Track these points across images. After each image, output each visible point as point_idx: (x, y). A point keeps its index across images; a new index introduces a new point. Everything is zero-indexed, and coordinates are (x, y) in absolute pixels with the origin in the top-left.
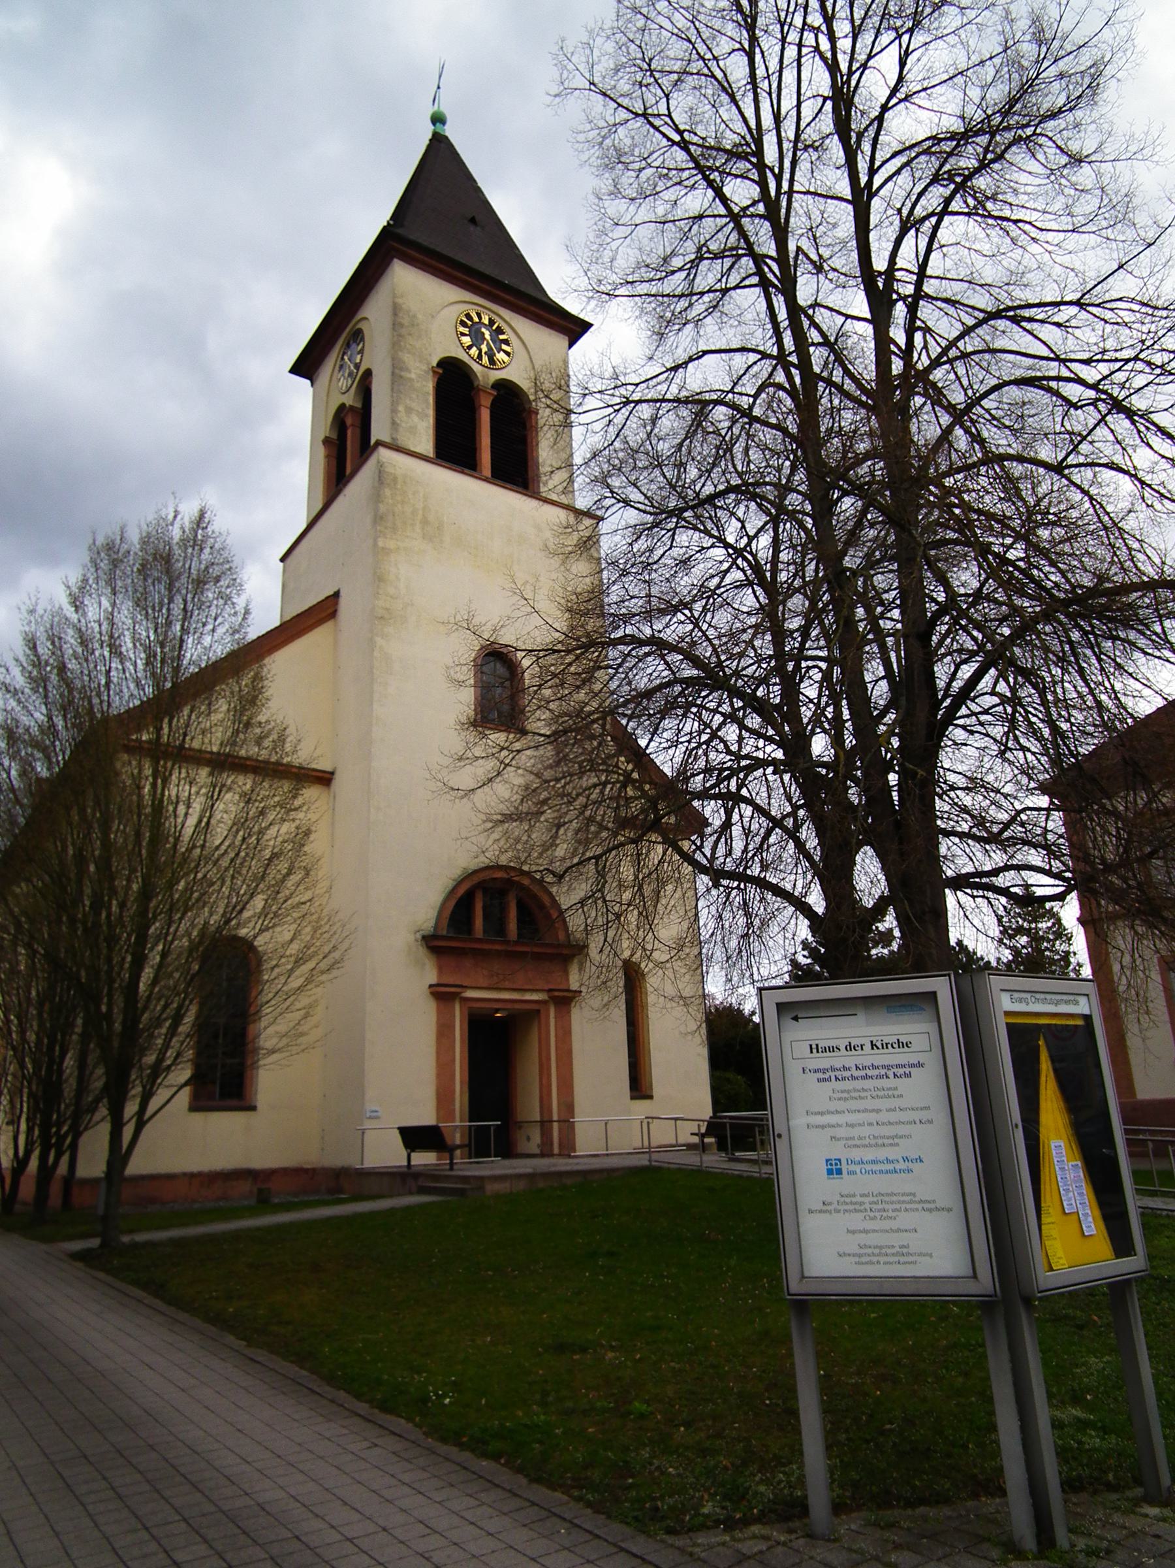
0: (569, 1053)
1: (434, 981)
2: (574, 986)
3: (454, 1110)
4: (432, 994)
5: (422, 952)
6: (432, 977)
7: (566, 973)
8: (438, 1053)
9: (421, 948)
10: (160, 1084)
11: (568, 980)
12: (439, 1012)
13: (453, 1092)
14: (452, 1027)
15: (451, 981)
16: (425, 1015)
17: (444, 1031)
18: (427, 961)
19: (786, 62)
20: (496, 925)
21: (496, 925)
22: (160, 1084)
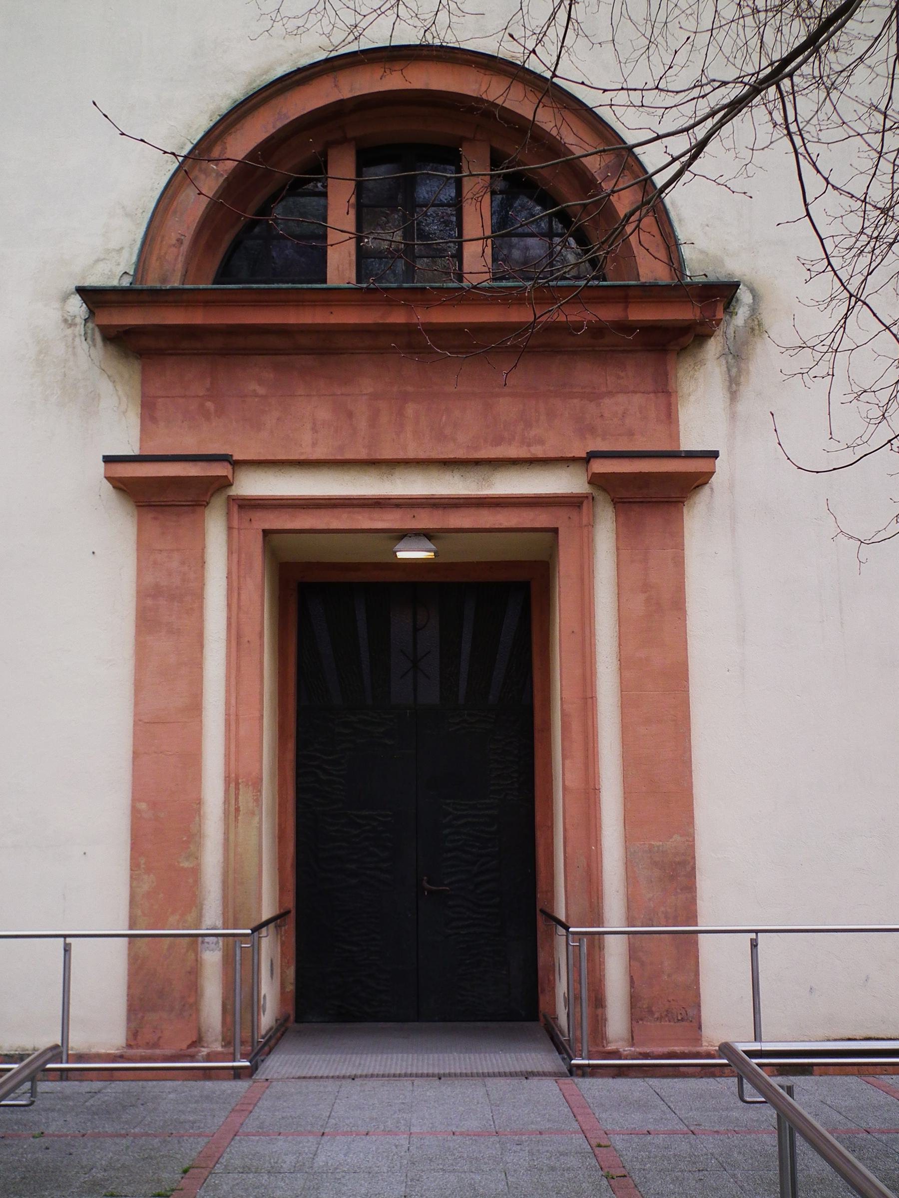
0: (677, 677)
1: (127, 442)
2: (691, 439)
3: (196, 872)
4: (122, 486)
5: (86, 357)
6: (121, 430)
7: (666, 394)
8: (139, 687)
9: (83, 347)
10: (334, 395)
11: (670, 417)
12: (143, 547)
13: (195, 807)
14: (191, 597)
15: (189, 444)
16: (96, 557)
17: (164, 609)
18: (105, 387)
19: (790, 121)
20: (410, 259)
21: (410, 259)
22: (334, 395)
